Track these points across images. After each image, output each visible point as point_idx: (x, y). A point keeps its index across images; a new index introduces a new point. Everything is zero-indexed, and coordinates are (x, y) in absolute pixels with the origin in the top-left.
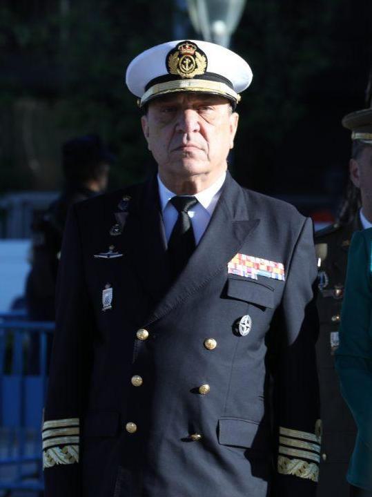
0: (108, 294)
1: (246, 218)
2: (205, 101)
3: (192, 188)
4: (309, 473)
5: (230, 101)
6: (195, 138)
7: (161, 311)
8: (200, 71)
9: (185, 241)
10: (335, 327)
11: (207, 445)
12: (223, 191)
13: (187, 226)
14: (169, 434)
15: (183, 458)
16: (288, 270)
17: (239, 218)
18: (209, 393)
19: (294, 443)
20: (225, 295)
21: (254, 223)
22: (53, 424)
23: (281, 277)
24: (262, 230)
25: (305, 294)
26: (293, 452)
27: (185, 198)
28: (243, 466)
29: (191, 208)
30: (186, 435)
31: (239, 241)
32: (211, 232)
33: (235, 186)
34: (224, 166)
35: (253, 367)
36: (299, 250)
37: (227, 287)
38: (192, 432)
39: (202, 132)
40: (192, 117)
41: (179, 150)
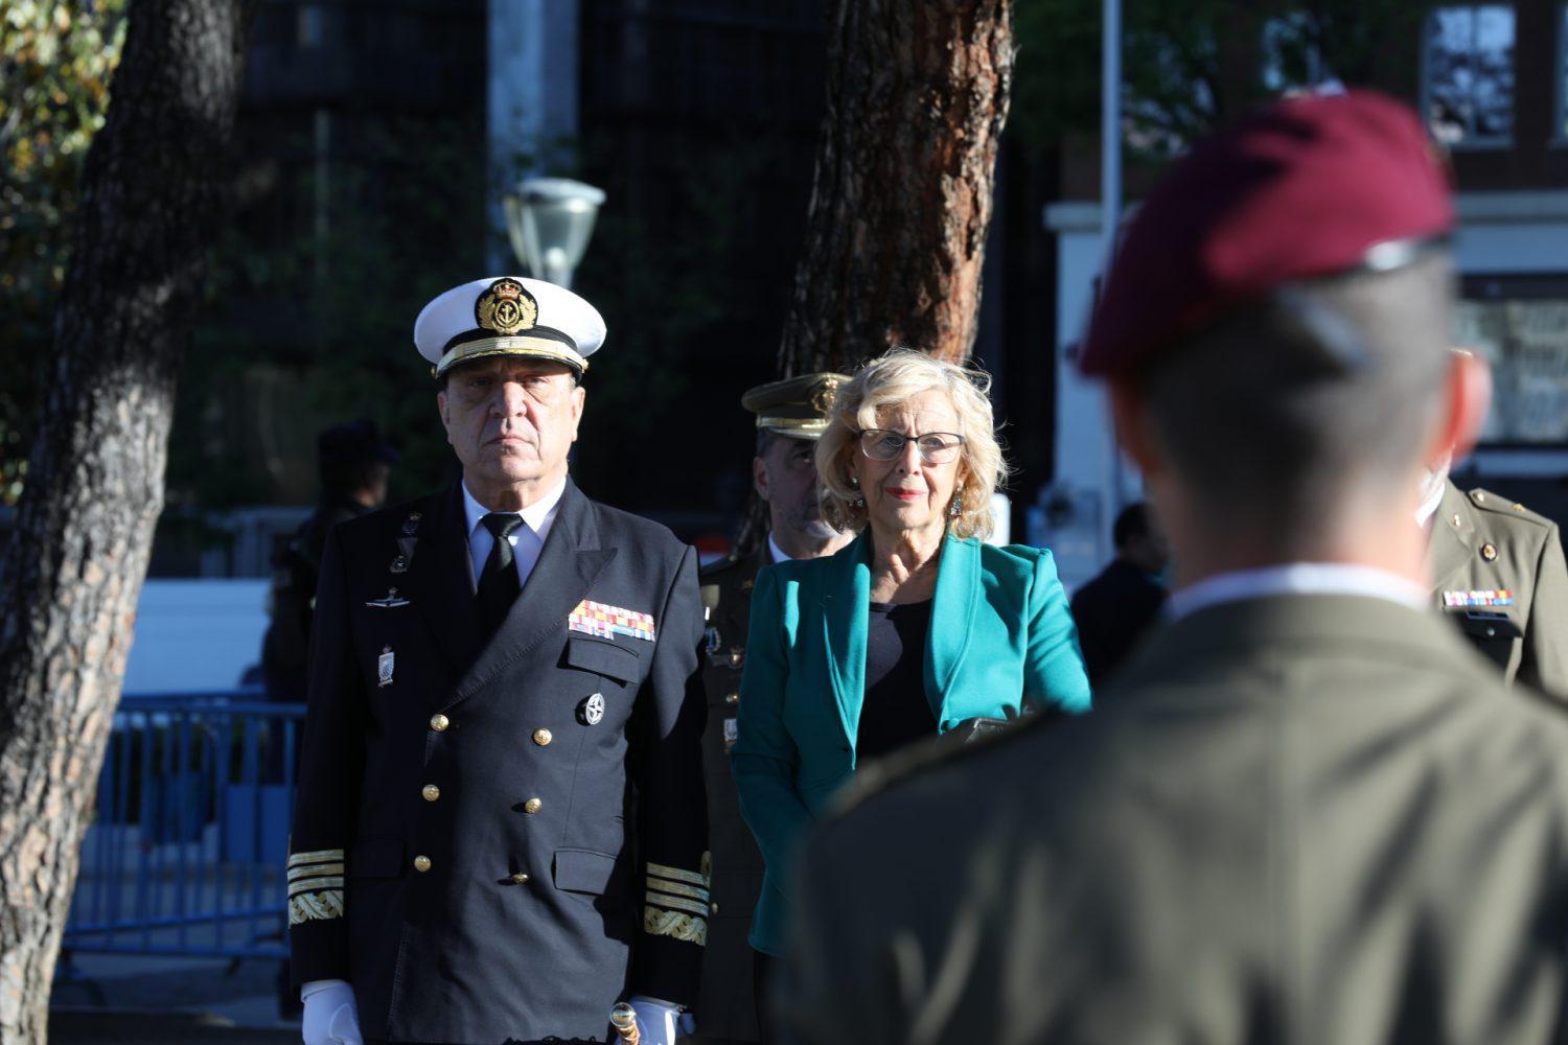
0: (387, 662)
1: (596, 546)
2: (534, 369)
3: (515, 501)
4: (692, 932)
5: (571, 368)
6: (520, 426)
7: (468, 687)
8: (526, 324)
9: (504, 581)
10: (731, 710)
11: (537, 890)
12: (561, 506)
13: (507, 559)
14: (480, 874)
15: (501, 910)
16: (659, 624)
17: (583, 547)
18: (540, 811)
19: (669, 887)
20: (564, 663)
21: (609, 554)
22: (515, 47)
23: (650, 636)
24: (621, 564)
25: (686, 662)
26: (667, 901)
27: (505, 516)
28: (591, 921)
29: (513, 531)
30: (506, 875)
31: (586, 582)
32: (544, 568)
33: (580, 498)
34: (564, 468)
35: (606, 773)
36: (676, 594)
37: (567, 652)
38: (514, 870)
39: (530, 416)
40: (515, 393)
41: (495, 444)
